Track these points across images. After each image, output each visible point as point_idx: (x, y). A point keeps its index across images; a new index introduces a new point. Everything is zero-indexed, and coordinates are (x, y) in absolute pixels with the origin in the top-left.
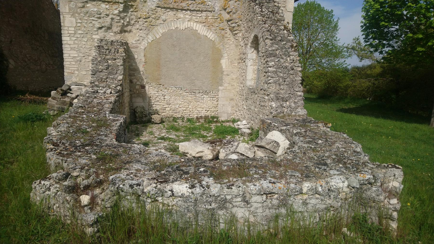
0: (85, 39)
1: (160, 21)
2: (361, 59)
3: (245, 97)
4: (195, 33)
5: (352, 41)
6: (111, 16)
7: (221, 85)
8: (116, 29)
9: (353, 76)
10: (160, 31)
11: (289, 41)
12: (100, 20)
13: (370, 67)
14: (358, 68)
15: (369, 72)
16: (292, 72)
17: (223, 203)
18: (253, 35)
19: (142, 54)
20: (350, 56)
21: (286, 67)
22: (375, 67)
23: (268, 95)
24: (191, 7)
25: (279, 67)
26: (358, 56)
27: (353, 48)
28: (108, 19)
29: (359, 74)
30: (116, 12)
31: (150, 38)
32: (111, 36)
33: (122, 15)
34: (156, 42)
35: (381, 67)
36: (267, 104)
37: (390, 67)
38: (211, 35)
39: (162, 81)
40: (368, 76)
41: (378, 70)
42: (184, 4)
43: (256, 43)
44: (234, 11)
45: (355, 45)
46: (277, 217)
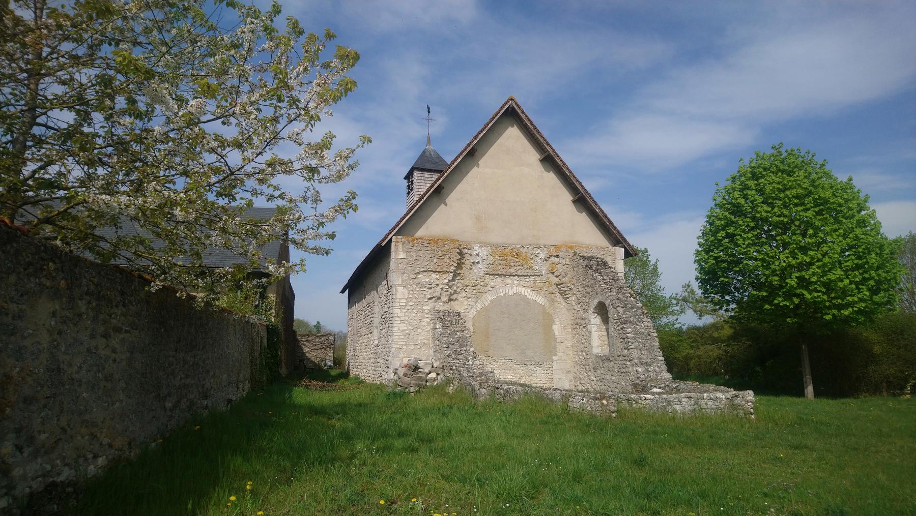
0: (415, 311)
1: (488, 288)
2: (701, 316)
3: (592, 366)
4: (524, 298)
5: (681, 289)
6: (441, 286)
7: (555, 355)
8: (445, 298)
9: (693, 342)
10: (489, 297)
11: (638, 308)
12: (430, 291)
13: (714, 326)
14: (697, 328)
15: (716, 335)
16: (649, 337)
17: (669, 403)
18: (596, 302)
19: (471, 324)
20: (682, 311)
21: (643, 333)
22: (723, 328)
23: (630, 361)
24: (519, 273)
25: (636, 333)
26: (695, 311)
27: (685, 300)
28: (438, 289)
29: (702, 338)
30: (446, 281)
31: (479, 306)
32: (440, 306)
33: (450, 284)
34: (485, 309)
35: (731, 327)
36: (630, 370)
37: (742, 328)
38: (540, 300)
39: (490, 353)
40: (715, 341)
41: (728, 331)
42: (512, 270)
43: (602, 310)
44: (563, 274)
45: (687, 294)
46: (695, 410)
